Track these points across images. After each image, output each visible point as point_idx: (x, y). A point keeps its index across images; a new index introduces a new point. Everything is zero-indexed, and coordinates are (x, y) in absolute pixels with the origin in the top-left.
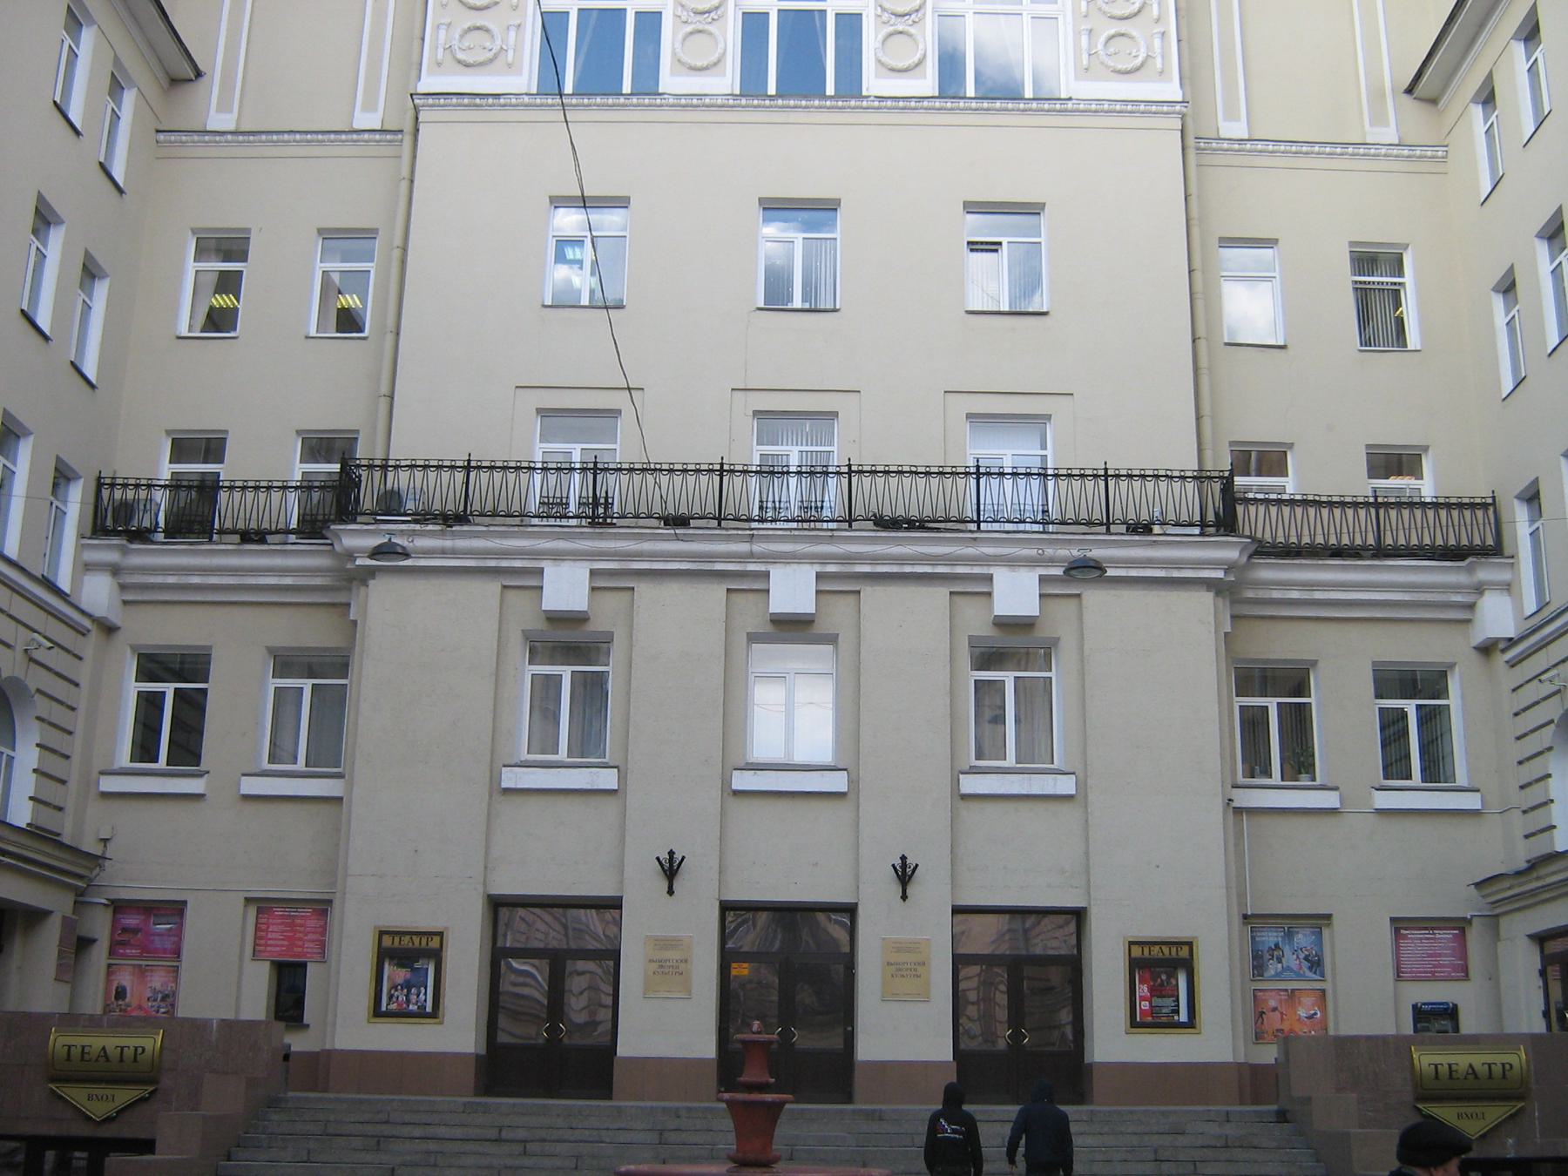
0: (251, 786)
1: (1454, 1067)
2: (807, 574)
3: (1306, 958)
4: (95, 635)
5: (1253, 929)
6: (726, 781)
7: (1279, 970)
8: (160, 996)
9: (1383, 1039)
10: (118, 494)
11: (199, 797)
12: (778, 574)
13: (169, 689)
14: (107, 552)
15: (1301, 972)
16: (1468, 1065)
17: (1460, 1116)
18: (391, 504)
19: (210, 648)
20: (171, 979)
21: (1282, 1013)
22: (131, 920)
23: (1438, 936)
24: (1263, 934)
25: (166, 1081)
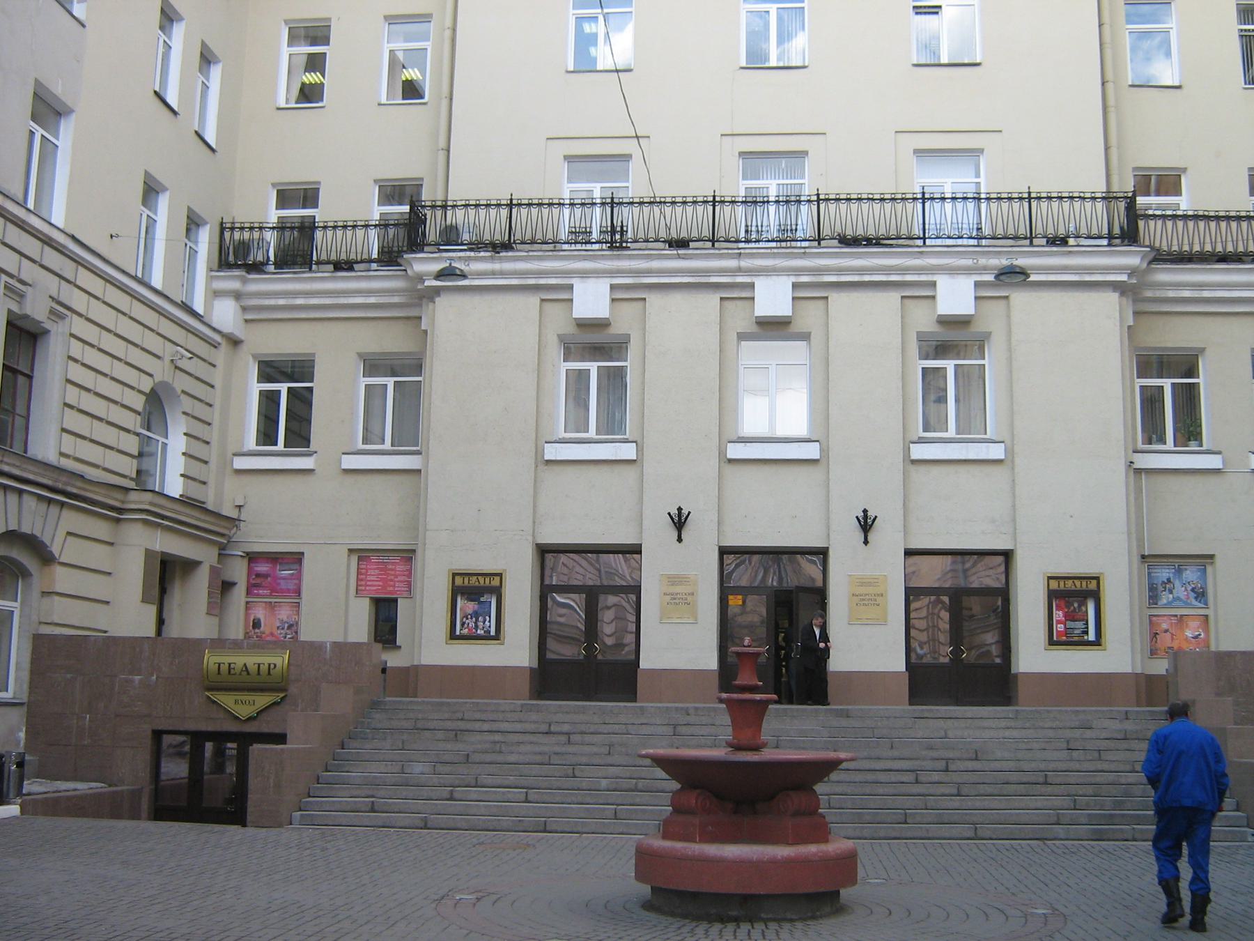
0: (350, 462)
3: (1193, 590)
4: (224, 346)
6: (722, 452)
7: (1170, 600)
8: (286, 625)
10: (237, 235)
11: (309, 471)
12: (761, 284)
13: (283, 388)
14: (231, 281)
18: (450, 236)
19: (314, 355)
20: (295, 612)
22: (262, 568)
25: (293, 689)
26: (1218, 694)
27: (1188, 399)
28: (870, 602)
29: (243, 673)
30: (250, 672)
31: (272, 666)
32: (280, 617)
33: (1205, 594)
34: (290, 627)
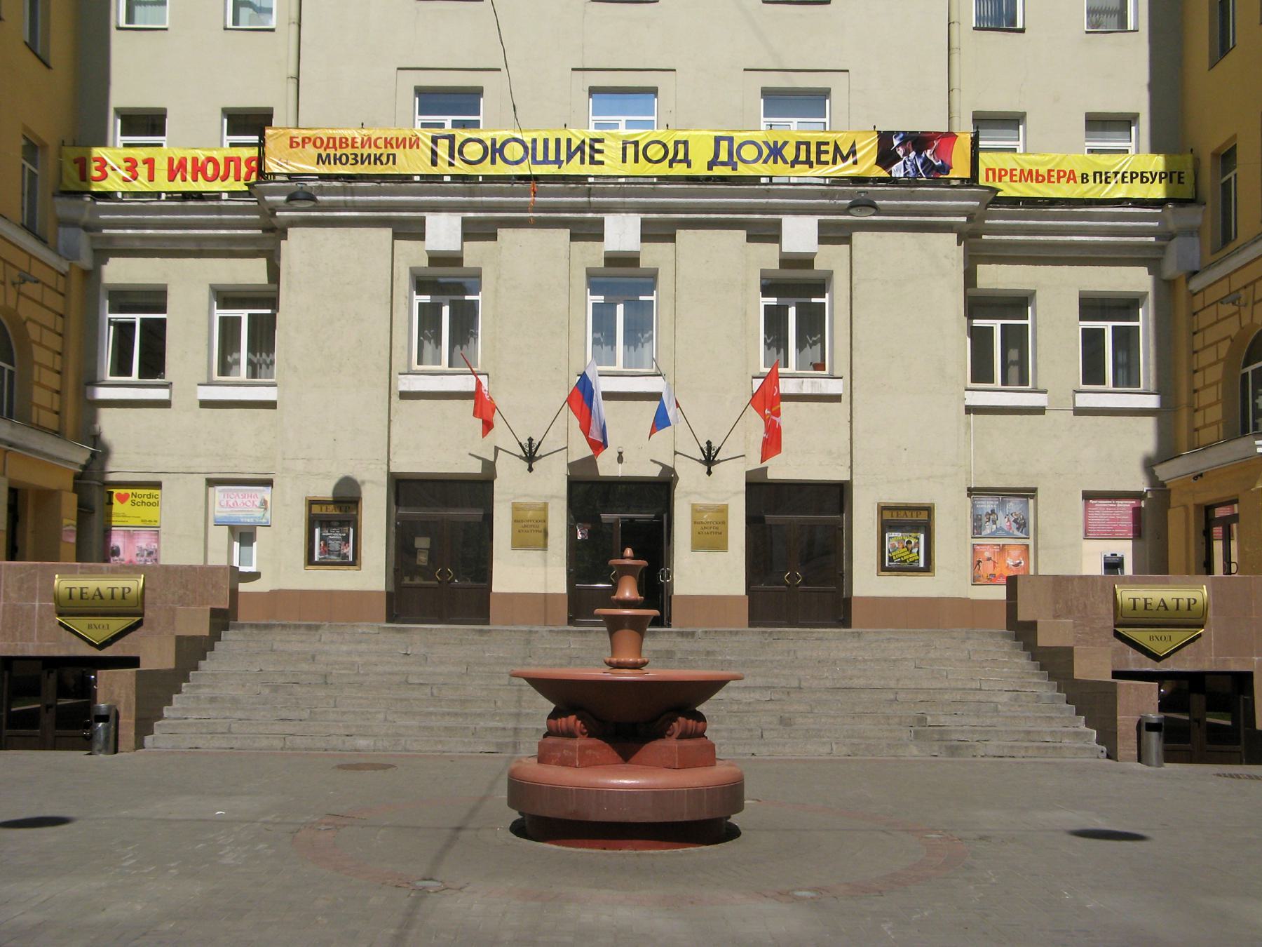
1: (1149, 601)
2: (634, 221)
3: (1015, 521)
5: (975, 499)
7: (993, 530)
8: (146, 553)
9: (192, 568)
15: (1011, 531)
16: (96, 588)
17: (1151, 638)
19: (166, 285)
20: (154, 540)
21: (995, 562)
23: (1118, 505)
24: (983, 502)
26: (1056, 617)
27: (1015, 338)
28: (532, 528)
29: (96, 597)
30: (104, 597)
31: (1192, 601)
32: (139, 544)
33: (1027, 525)
34: (150, 554)
